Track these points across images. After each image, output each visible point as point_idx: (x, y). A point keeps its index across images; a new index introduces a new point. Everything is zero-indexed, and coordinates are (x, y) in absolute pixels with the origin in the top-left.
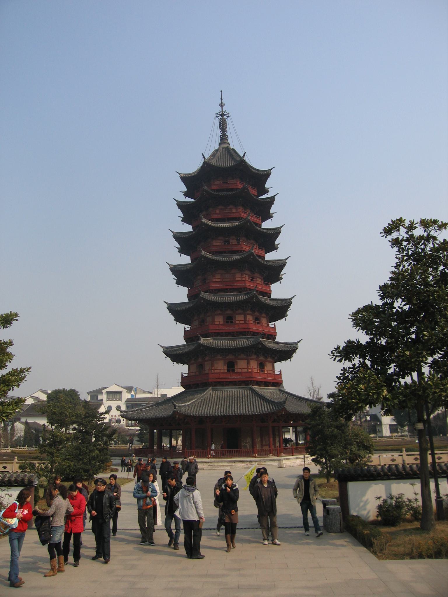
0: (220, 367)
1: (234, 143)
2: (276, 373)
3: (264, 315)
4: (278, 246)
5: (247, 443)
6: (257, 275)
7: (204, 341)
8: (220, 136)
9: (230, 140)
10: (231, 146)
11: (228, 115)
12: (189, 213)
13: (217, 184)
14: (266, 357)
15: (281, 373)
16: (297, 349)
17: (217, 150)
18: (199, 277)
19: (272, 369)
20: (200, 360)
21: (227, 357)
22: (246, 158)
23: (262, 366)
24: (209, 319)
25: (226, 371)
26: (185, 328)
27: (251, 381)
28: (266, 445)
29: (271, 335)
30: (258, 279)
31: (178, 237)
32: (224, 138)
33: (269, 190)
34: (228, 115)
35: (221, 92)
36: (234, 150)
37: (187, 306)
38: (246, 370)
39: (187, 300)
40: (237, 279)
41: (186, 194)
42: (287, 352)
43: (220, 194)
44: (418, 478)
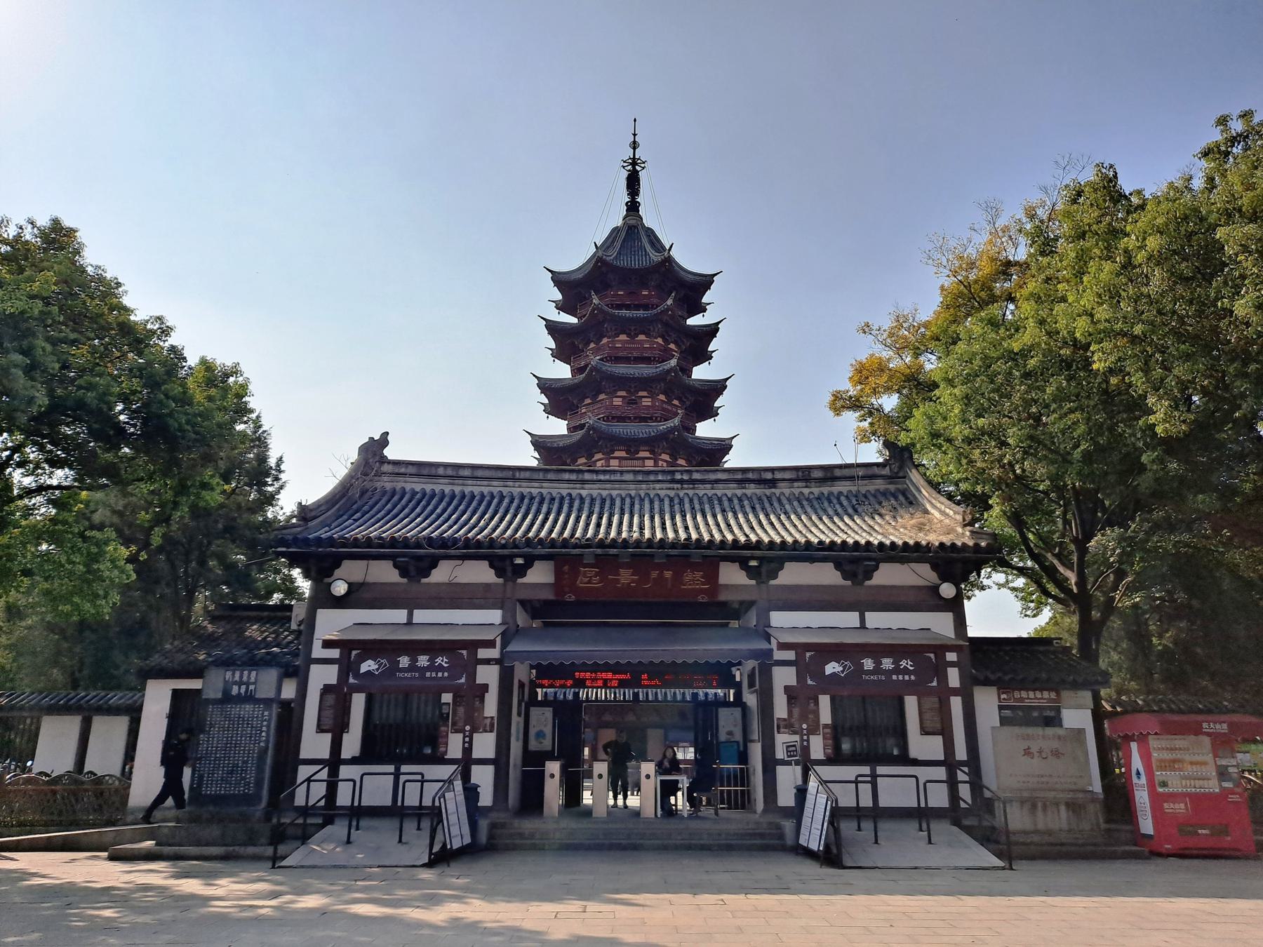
1: (649, 218)
9: (642, 211)
12: (566, 343)
31: (546, 386)
32: (633, 207)
41: (561, 307)
43: (624, 312)
44: (494, 801)
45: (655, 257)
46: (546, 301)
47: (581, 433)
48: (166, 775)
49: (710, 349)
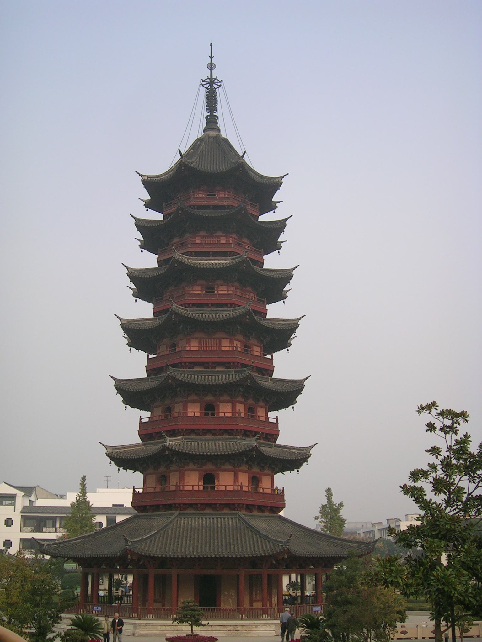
0: (193, 481)
1: (227, 130)
2: (270, 420)
3: (261, 403)
4: (282, 245)
5: (227, 602)
6: (253, 341)
7: (170, 442)
8: (206, 117)
10: (223, 134)
11: (219, 84)
13: (200, 197)
14: (262, 468)
16: (309, 457)
17: (200, 140)
18: (165, 340)
19: (270, 486)
20: (162, 469)
21: (204, 467)
22: (246, 158)
23: (255, 480)
24: (178, 408)
25: (201, 488)
26: (141, 419)
27: (239, 504)
28: (258, 601)
29: (266, 370)
30: (255, 348)
31: (141, 226)
32: (212, 122)
33: (277, 205)
34: (219, 84)
35: (211, 45)
36: (226, 141)
37: (156, 273)
38: (231, 488)
39: (162, 219)
40: (223, 349)
41: (149, 205)
42: (295, 460)
46: (136, 204)
47: (165, 316)
49: (274, 199)
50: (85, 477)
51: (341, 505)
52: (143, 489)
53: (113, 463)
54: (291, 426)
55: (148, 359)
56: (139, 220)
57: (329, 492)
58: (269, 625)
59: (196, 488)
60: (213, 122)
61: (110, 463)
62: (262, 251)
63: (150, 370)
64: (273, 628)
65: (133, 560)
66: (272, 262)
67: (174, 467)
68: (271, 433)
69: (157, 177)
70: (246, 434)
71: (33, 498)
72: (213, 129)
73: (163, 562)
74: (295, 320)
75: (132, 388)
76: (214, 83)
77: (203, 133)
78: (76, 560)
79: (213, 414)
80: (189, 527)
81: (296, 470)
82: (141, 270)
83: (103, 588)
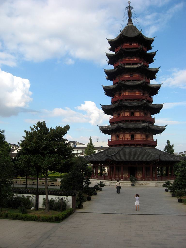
2: (152, 117)
7: (119, 125)
11: (132, 8)
15: (156, 140)
18: (117, 93)
20: (117, 133)
21: (131, 133)
25: (130, 139)
26: (110, 118)
29: (150, 101)
31: (109, 56)
34: (132, 8)
41: (110, 50)
42: (160, 130)
45: (137, 34)
47: (117, 85)
48: (11, 73)
49: (151, 46)
50: (91, 137)
51: (173, 146)
52: (111, 140)
53: (101, 132)
54: (159, 120)
55: (112, 98)
56: (108, 54)
57: (168, 142)
58: (153, 183)
59: (128, 139)
60: (130, 21)
61: (101, 132)
62: (148, 62)
63: (113, 102)
64: (154, 184)
65: (109, 162)
66: (151, 66)
67: (121, 133)
68: (153, 121)
69: (113, 40)
70: (144, 122)
71: (75, 145)
72: (131, 23)
73: (118, 163)
74: (160, 85)
75: (107, 108)
76: (130, 8)
77: (127, 25)
78: (92, 162)
79: (133, 116)
80: (126, 152)
81: (160, 134)
82: (109, 70)
83: (120, 184)
